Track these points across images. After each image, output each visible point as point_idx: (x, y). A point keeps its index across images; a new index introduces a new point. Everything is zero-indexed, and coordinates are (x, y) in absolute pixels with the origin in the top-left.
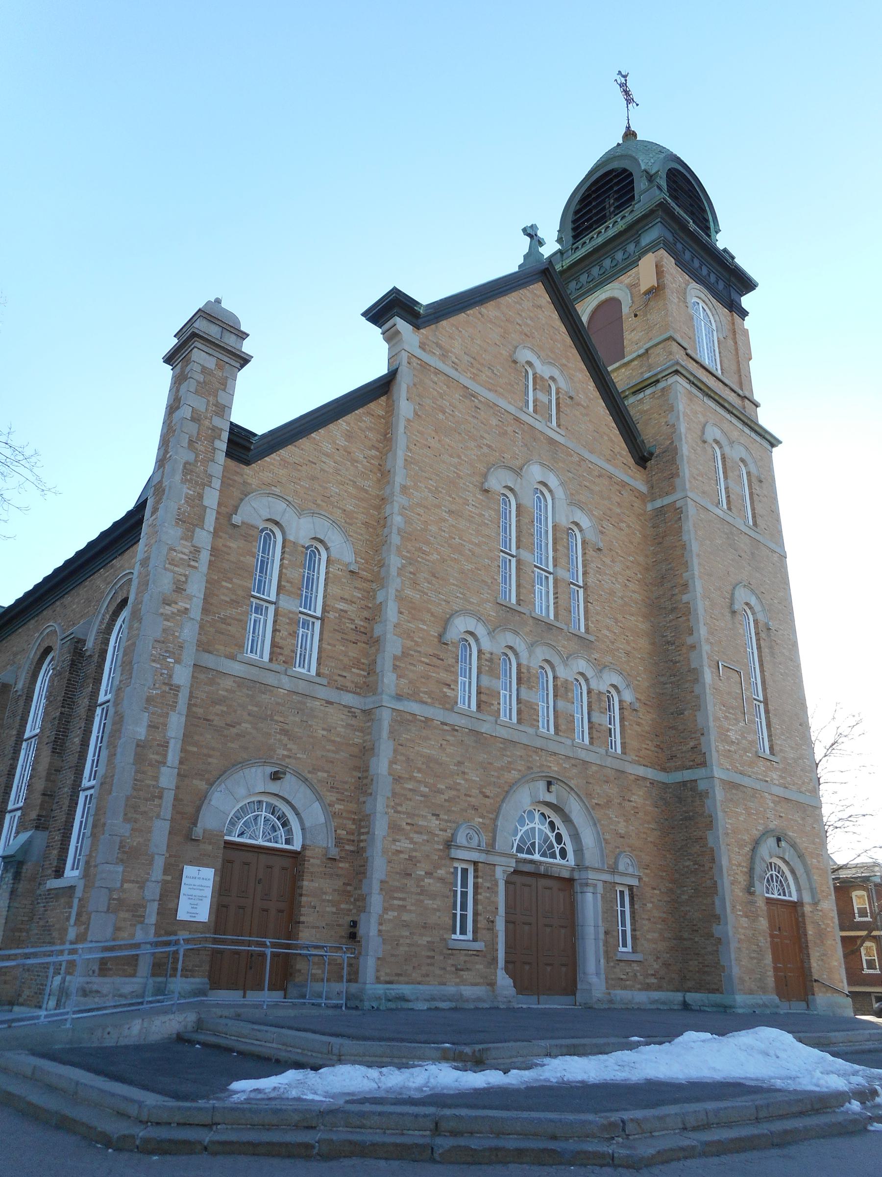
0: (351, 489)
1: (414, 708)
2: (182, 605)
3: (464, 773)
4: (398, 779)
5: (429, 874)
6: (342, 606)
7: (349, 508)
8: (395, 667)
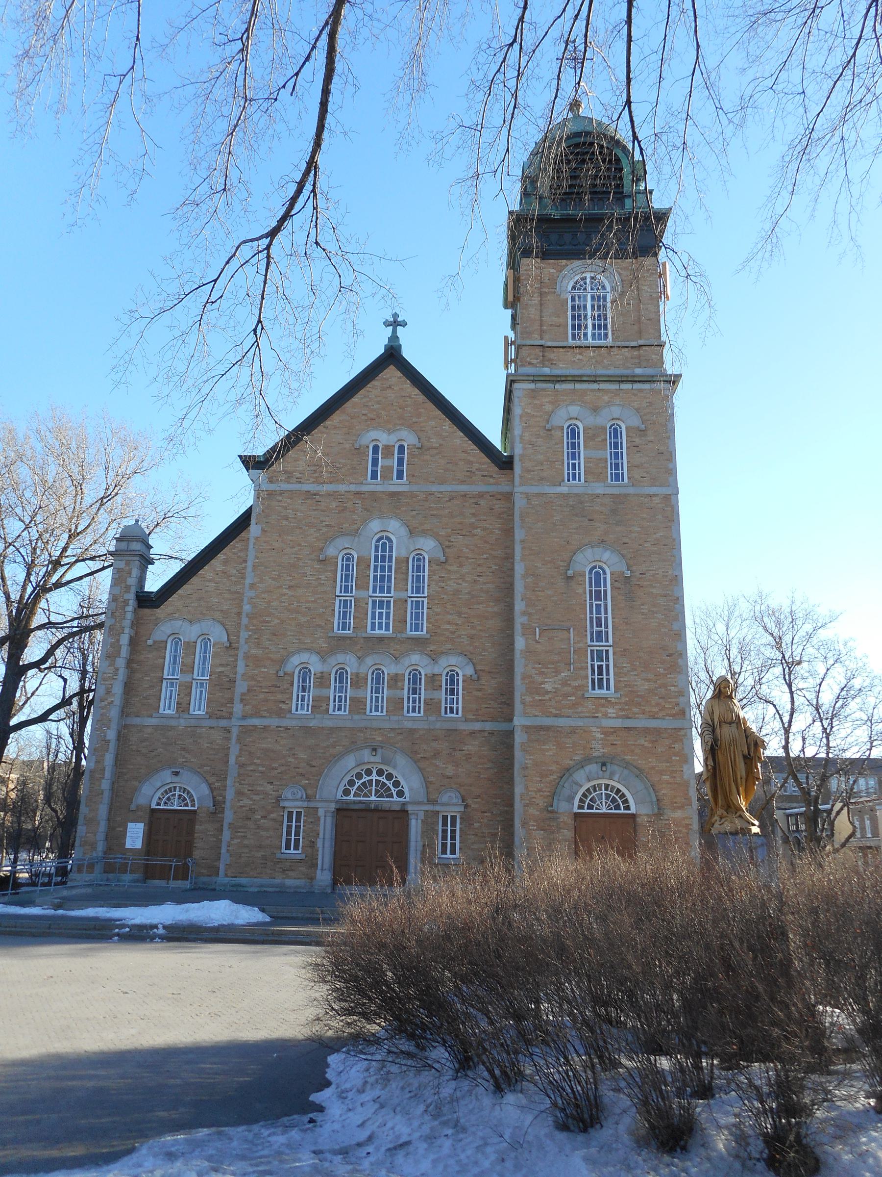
0: (227, 596)
1: (256, 722)
2: (110, 700)
3: (294, 754)
4: (242, 766)
5: (264, 817)
6: (221, 669)
7: (225, 608)
8: (242, 700)
